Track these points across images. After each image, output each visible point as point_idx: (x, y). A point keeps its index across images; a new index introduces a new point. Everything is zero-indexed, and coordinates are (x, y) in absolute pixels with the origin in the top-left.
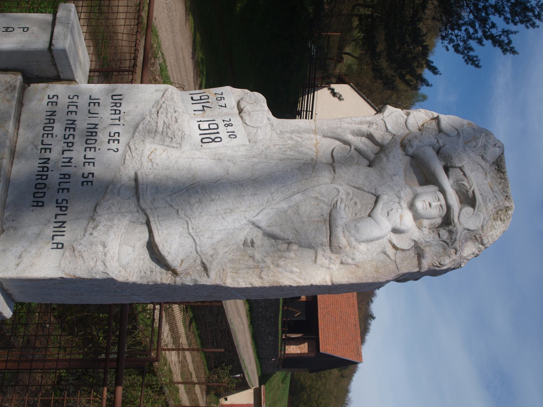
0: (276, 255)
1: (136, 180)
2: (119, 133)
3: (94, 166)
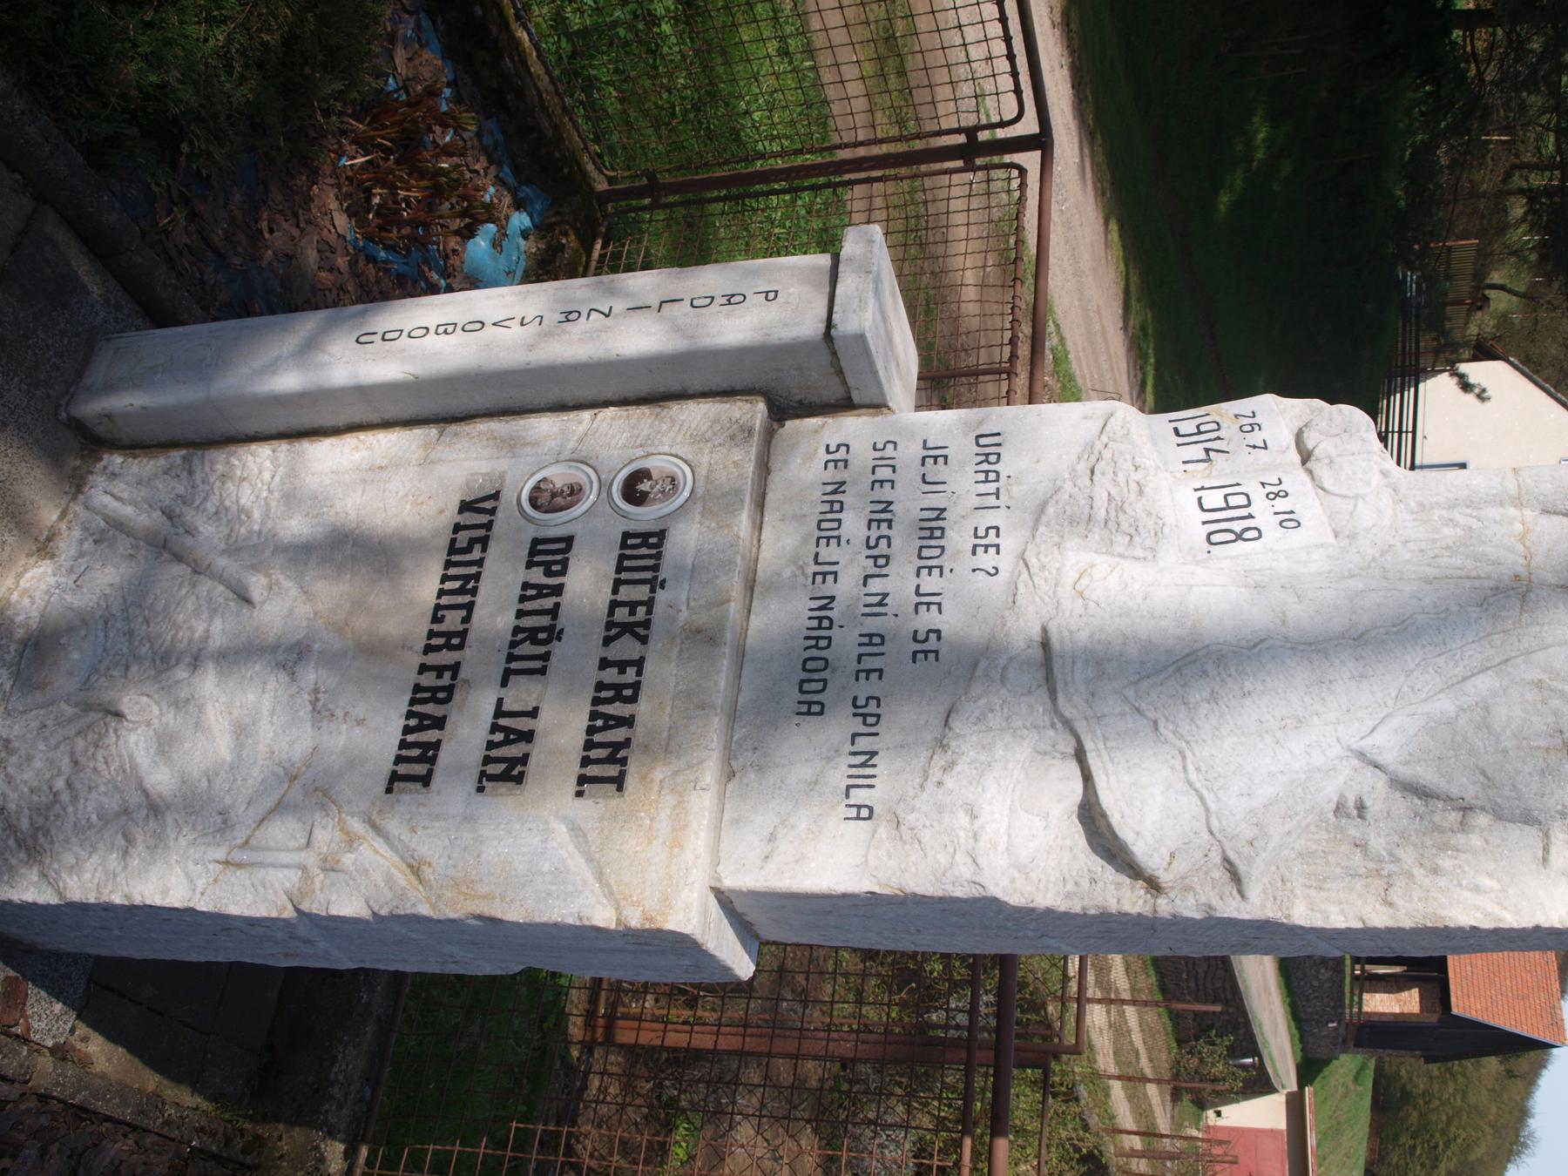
0: (1429, 843)
1: (1045, 644)
2: (997, 528)
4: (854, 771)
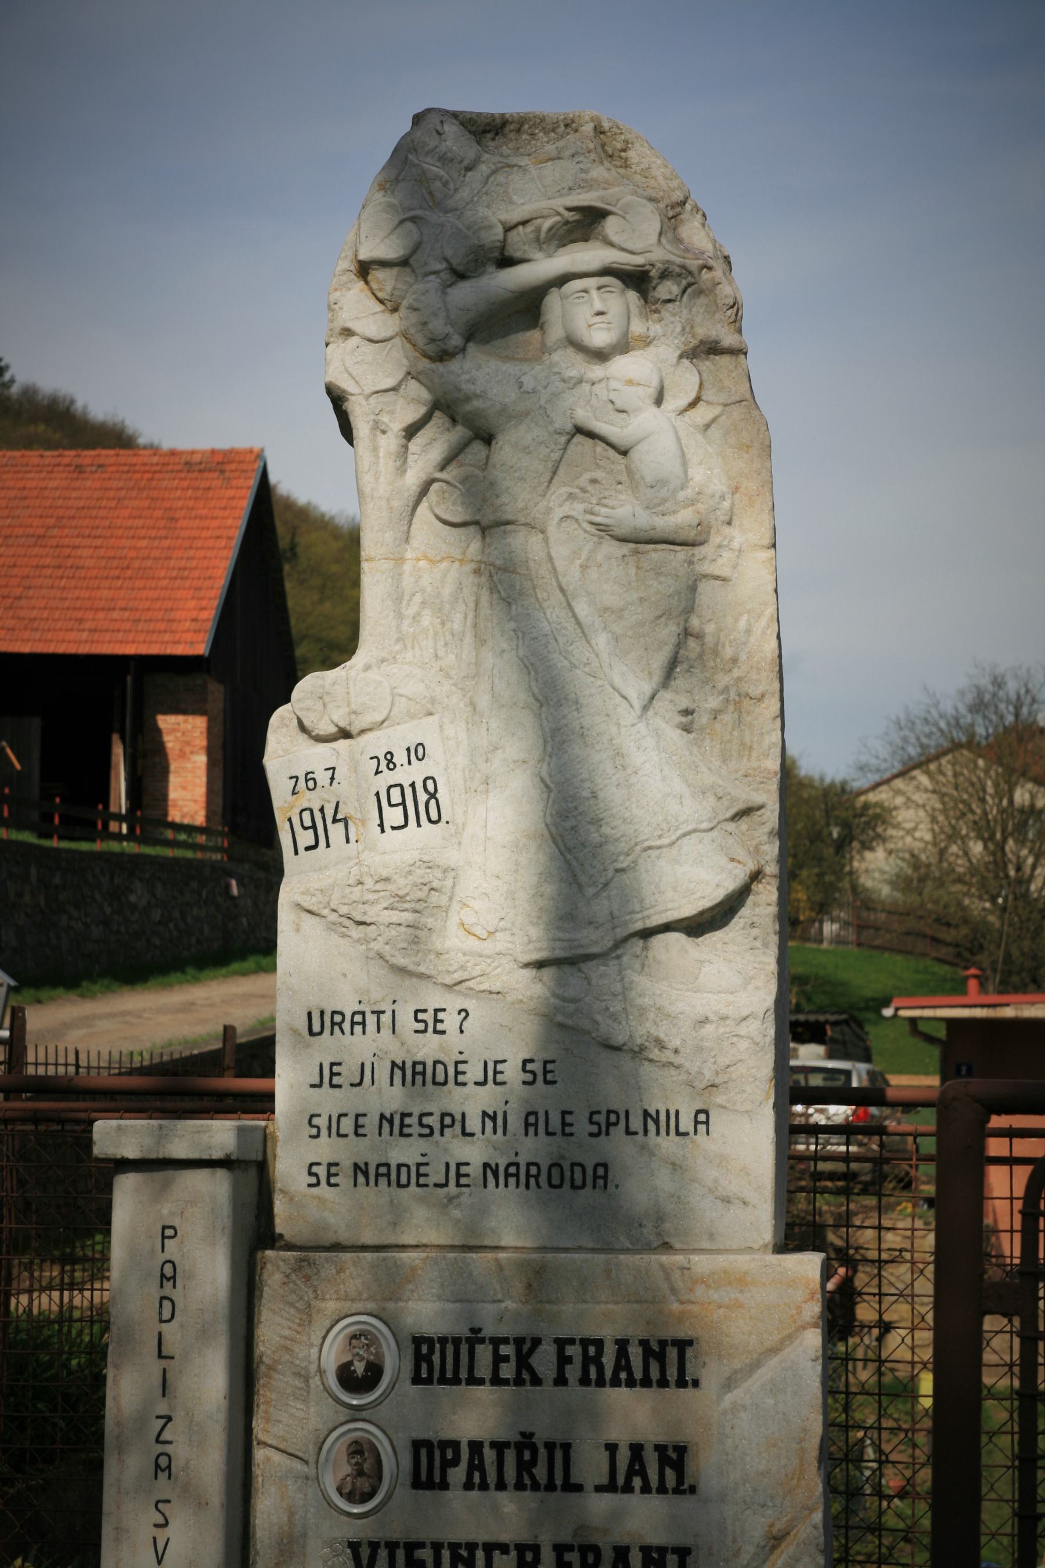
0: (712, 664)
1: (540, 965)
2: (416, 1012)
3: (504, 1061)
4: (663, 1130)
